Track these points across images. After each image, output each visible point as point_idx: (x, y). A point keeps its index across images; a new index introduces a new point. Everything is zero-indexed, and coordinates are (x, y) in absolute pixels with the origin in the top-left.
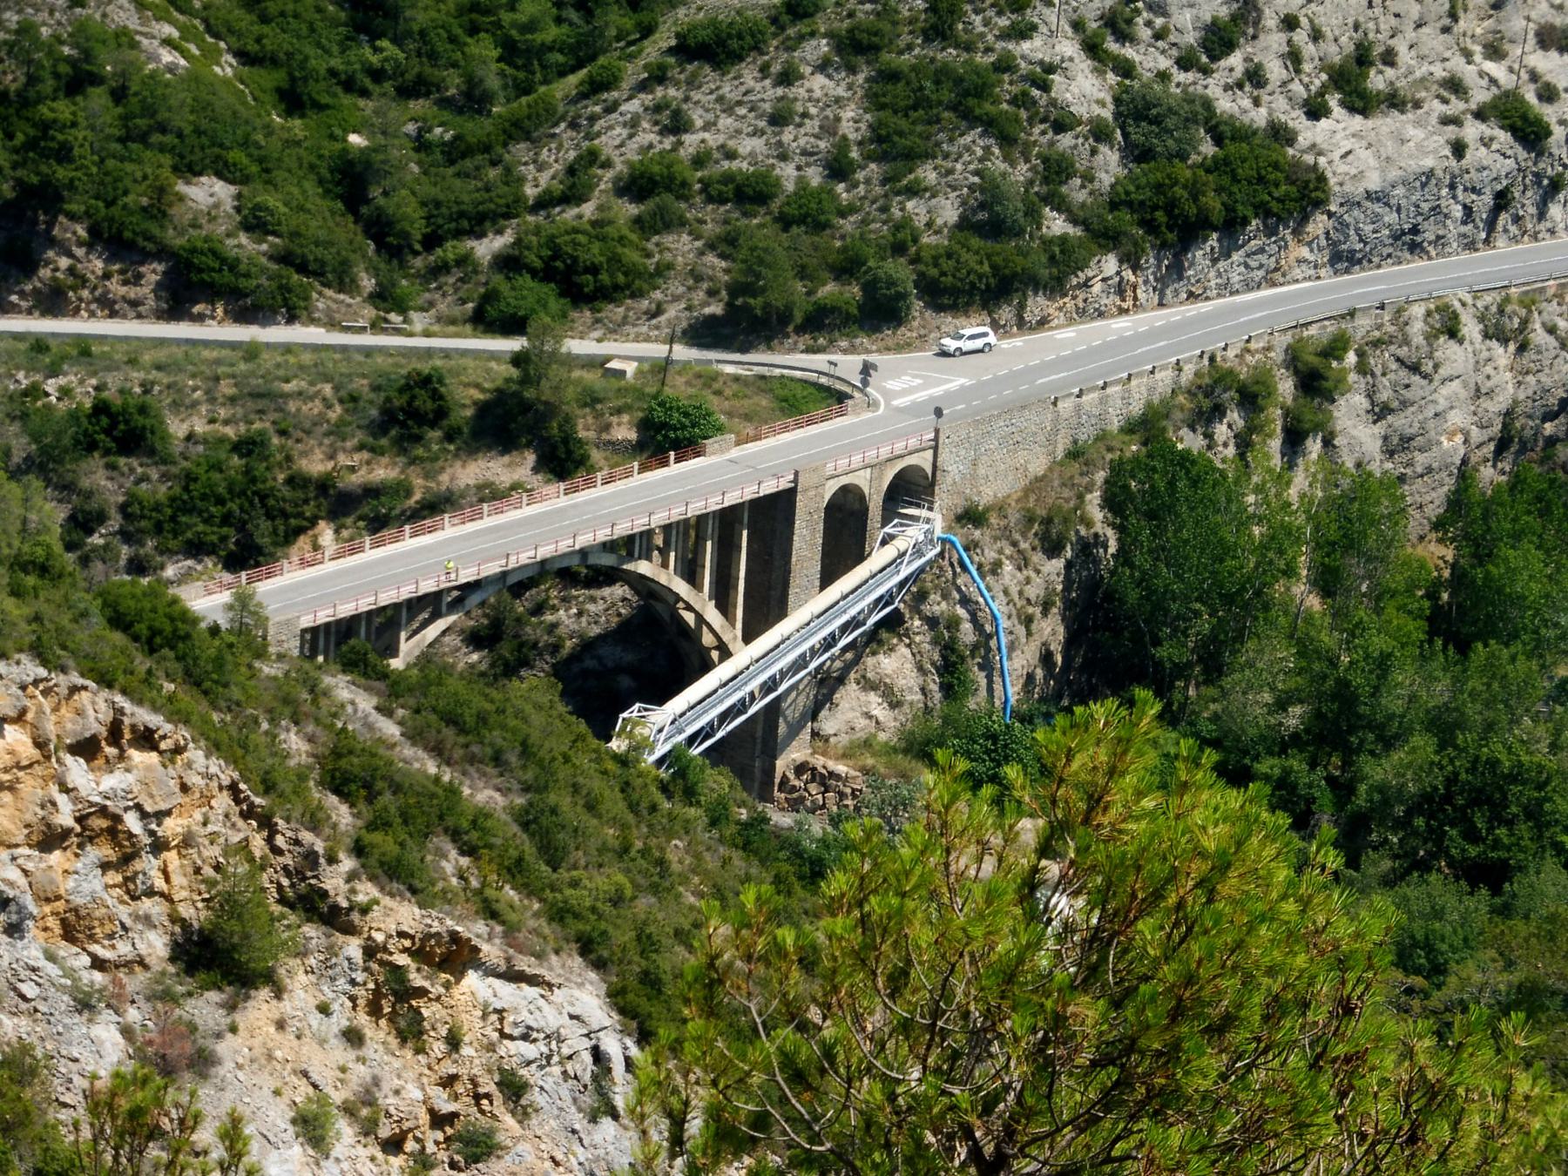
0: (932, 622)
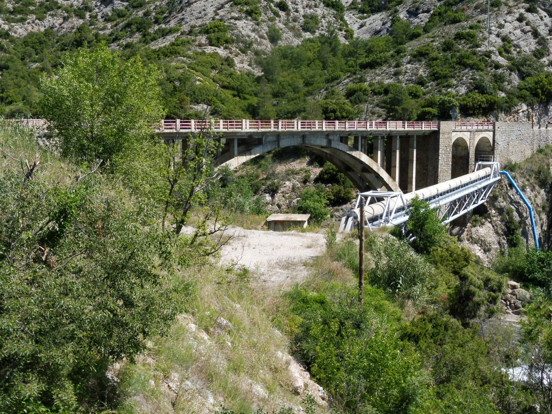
0: (500, 211)
